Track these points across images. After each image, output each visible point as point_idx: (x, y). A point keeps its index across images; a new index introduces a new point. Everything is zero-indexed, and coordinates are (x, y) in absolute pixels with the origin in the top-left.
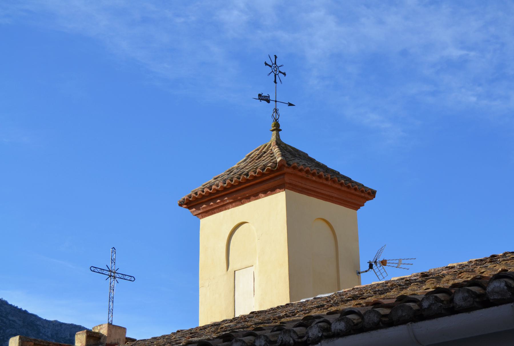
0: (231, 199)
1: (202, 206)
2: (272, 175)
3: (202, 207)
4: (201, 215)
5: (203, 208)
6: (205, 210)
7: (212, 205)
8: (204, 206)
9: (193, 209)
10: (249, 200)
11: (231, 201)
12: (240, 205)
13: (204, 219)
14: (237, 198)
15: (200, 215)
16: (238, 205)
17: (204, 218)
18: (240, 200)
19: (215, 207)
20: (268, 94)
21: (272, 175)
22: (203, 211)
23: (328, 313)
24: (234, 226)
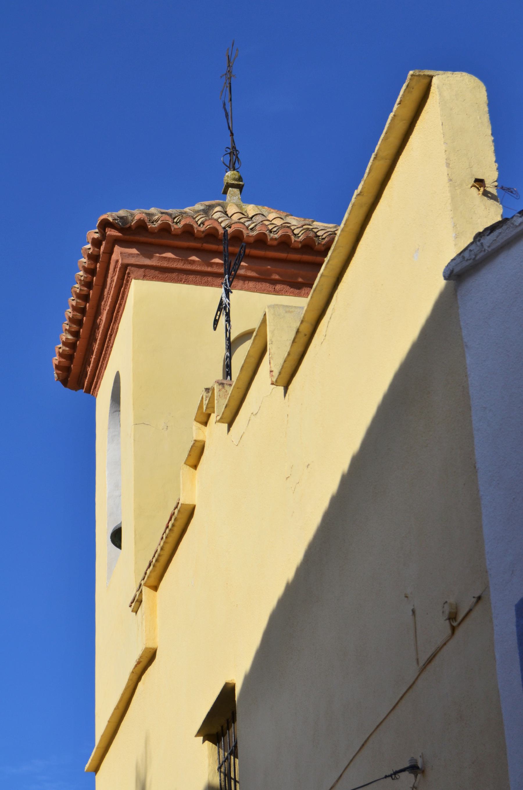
0: (253, 271)
1: (164, 253)
2: (283, 255)
3: (164, 255)
4: (144, 272)
5: (162, 257)
6: (165, 264)
7: (194, 262)
8: (169, 255)
9: (132, 248)
10: (297, 291)
11: (253, 274)
12: (269, 292)
13: (145, 282)
14: (234, 271)
15: (143, 270)
16: (216, 285)
17: (147, 280)
18: (274, 282)
19: (198, 268)
20: (221, 77)
21: (283, 255)
22: (159, 264)
23: (235, 701)
24: (244, 331)
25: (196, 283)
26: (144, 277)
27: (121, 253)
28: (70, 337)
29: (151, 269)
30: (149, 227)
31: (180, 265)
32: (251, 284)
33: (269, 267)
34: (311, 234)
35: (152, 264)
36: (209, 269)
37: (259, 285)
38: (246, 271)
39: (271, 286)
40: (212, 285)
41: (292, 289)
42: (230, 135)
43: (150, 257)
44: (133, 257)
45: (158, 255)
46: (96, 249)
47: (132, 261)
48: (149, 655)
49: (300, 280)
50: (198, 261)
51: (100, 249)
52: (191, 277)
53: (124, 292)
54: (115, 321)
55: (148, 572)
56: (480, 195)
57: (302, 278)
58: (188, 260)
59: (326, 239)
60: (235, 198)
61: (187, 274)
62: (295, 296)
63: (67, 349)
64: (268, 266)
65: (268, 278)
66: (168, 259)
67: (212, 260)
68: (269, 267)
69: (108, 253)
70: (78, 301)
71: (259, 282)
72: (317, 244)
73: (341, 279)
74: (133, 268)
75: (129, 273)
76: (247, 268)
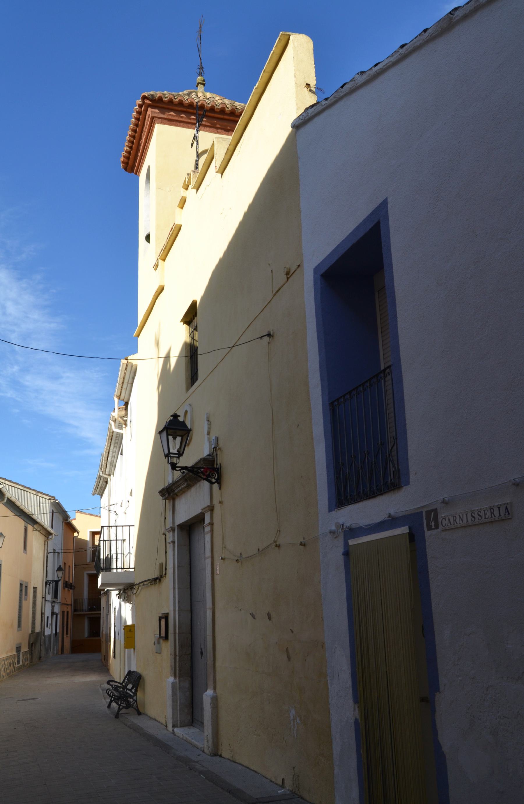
6: (170, 118)
15: (161, 119)
18: (217, 128)
26: (161, 123)
28: (128, 149)
30: (164, 100)
32: (208, 129)
33: (216, 121)
34: (234, 108)
43: (164, 114)
44: (157, 113)
46: (140, 109)
47: (156, 115)
48: (161, 288)
49: (229, 128)
50: (185, 117)
51: (142, 109)
52: (182, 124)
53: (152, 129)
54: (148, 142)
55: (161, 253)
59: (241, 110)
63: (127, 154)
69: (145, 111)
70: (132, 132)
71: (211, 128)
72: (236, 112)
73: (251, 120)
74: (156, 119)
75: (154, 121)
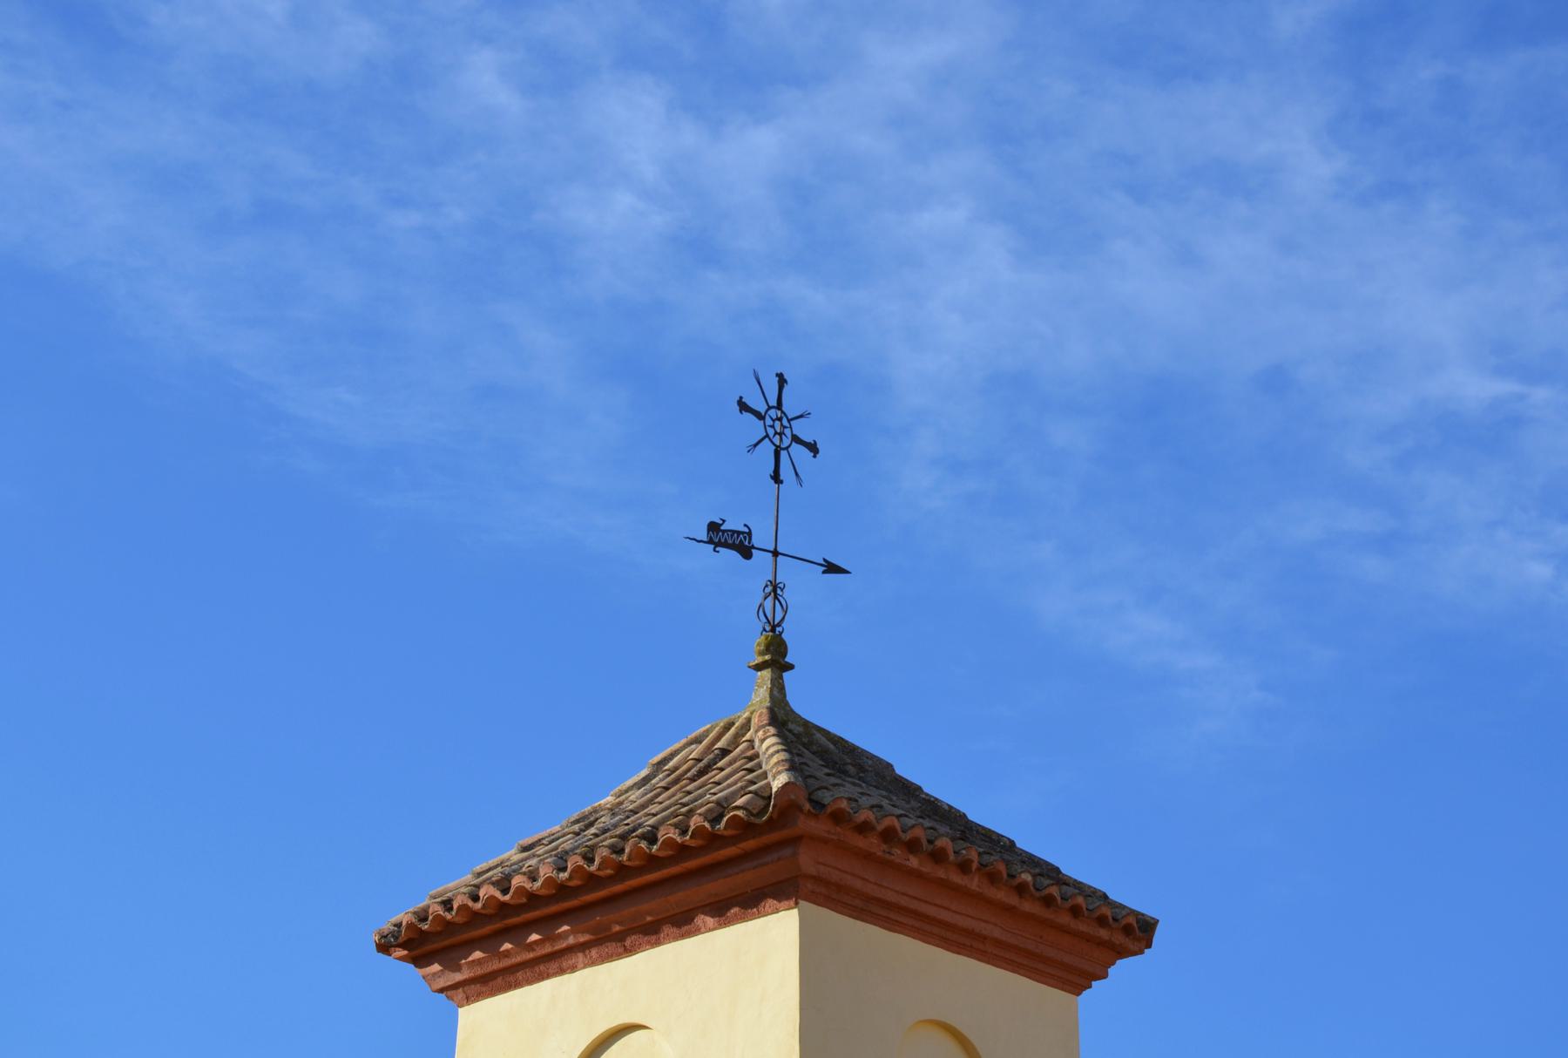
1: (470, 954)
3: (470, 959)
4: (464, 992)
5: (473, 961)
6: (479, 971)
8: (477, 955)
10: (654, 937)
11: (583, 938)
12: (619, 956)
13: (472, 1005)
15: (461, 990)
17: (473, 1002)
18: (620, 938)
25: (530, 982)
27: (424, 978)
29: (469, 984)
31: (496, 965)
35: (465, 977)
36: (531, 955)
37: (605, 949)
38: (574, 936)
39: (619, 944)
40: (548, 976)
41: (646, 938)
42: (739, 413)
45: (463, 961)
56: (440, 911)
57: (651, 915)
58: (500, 953)
60: (762, 690)
61: (513, 973)
62: (629, 951)
64: (561, 926)
65: (608, 933)
66: (479, 962)
67: (500, 947)
68: (598, 918)
76: (572, 932)
